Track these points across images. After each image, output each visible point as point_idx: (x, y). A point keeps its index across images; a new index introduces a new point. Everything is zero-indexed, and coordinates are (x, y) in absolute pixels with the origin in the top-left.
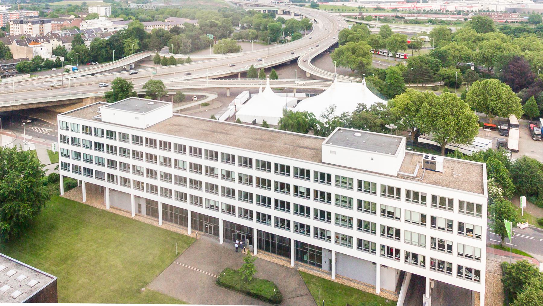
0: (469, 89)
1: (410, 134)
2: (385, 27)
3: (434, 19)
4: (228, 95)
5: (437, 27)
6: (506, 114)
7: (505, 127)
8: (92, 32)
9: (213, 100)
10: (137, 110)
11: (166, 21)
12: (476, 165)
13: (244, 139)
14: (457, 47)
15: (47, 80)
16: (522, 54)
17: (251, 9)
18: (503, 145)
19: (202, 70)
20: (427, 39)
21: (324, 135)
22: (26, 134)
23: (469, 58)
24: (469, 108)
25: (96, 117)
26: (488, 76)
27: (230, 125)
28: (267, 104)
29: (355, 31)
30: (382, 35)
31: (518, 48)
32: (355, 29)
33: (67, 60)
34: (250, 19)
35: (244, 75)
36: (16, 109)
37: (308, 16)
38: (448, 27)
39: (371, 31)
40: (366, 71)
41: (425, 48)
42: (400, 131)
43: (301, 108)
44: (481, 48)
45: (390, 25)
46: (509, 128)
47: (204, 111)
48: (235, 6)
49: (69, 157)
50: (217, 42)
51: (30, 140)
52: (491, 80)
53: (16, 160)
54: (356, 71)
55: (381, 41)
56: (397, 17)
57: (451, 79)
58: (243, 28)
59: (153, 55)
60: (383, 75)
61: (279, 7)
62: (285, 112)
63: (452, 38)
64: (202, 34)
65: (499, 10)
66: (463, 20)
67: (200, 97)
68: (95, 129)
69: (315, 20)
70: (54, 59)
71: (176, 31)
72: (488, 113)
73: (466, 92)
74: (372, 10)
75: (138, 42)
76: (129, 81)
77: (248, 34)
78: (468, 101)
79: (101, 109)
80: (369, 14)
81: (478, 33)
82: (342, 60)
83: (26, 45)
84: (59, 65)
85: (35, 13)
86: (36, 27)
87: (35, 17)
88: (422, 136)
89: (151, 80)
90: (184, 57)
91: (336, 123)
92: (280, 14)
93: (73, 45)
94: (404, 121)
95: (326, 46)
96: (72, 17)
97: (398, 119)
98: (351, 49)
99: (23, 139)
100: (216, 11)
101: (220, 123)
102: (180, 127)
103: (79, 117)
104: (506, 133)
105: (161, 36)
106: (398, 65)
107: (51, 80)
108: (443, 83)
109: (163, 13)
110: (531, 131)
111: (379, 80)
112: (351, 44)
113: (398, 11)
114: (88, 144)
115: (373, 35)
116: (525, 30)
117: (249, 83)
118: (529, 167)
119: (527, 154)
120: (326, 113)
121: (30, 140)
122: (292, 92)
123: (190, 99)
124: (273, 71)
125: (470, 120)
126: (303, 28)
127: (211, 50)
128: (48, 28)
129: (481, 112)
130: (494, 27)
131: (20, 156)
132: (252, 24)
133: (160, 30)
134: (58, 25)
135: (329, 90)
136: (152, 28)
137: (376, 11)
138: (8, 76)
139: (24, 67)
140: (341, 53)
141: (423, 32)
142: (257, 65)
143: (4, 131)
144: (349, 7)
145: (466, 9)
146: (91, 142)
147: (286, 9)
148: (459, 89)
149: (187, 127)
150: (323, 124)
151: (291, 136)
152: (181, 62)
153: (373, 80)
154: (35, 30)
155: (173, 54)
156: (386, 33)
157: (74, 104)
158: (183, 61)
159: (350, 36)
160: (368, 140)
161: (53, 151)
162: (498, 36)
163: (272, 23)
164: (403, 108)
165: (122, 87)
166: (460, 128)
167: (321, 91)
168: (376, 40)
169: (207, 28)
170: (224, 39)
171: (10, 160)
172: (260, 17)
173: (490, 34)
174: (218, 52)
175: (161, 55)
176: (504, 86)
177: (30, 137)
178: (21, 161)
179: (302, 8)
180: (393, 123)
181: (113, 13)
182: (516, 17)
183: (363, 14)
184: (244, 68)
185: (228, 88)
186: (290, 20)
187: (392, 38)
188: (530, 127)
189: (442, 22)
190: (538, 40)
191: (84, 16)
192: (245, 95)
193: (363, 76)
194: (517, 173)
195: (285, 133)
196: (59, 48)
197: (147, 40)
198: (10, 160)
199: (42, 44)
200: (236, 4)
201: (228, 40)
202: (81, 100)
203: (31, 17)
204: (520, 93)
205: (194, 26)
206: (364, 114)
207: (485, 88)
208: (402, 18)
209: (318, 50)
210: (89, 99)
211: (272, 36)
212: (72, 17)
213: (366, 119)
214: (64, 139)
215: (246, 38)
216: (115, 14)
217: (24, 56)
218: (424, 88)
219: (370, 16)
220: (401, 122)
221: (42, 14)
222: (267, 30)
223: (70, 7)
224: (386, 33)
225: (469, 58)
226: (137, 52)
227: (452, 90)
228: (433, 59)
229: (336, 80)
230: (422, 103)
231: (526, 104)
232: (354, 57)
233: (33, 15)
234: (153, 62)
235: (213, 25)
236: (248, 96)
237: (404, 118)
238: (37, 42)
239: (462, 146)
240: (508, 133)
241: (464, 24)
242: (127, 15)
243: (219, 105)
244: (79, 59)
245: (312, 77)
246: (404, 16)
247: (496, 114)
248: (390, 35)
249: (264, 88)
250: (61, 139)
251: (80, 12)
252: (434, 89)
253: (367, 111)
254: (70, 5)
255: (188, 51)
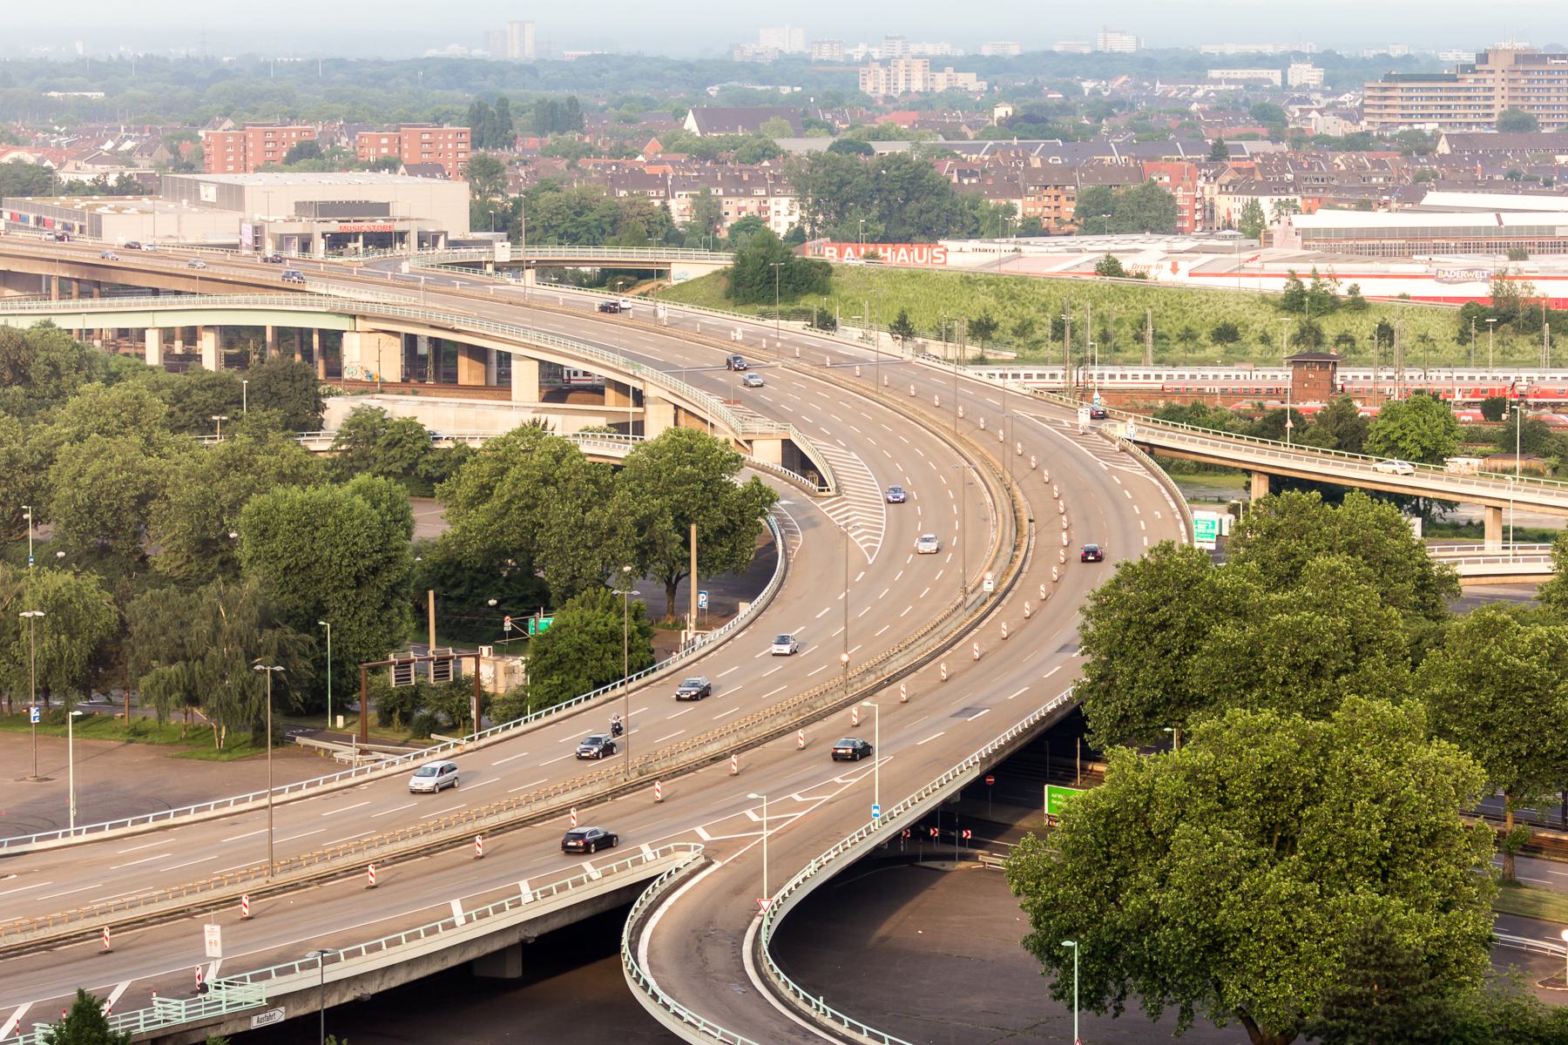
61: (363, 296)
69: (796, 459)
74: (1443, 329)
80: (1414, 378)
95: (941, 761)
98: (1242, 789)
112: (1245, 736)
137: (1489, 343)
144: (1178, 298)
151: (129, 251)
159: (1227, 632)
163: (296, 493)
168: (1513, 687)
172: (134, 416)
183: (1349, 376)
186: (503, 454)
209: (855, 810)
219: (1427, 402)
232: (1280, 881)
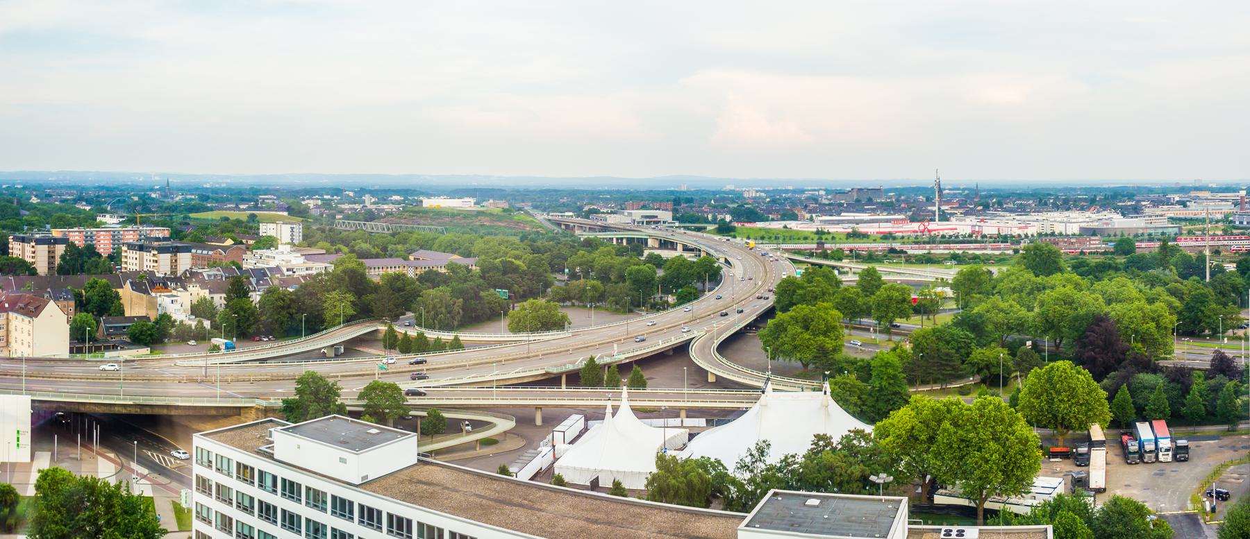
0: (1022, 385)
1: (920, 490)
2: (868, 270)
3: (960, 252)
4: (539, 422)
5: (965, 268)
6: (1084, 426)
7: (1083, 450)
8: (265, 275)
9: (505, 433)
10: (344, 443)
11: (411, 258)
12: (1036, 532)
13: (571, 521)
14: (1004, 305)
15: (179, 362)
16: (1107, 309)
17: (592, 235)
18: (1081, 483)
19: (478, 367)
20: (949, 292)
21: (746, 508)
22: (139, 463)
23: (1022, 325)
24: (1023, 422)
25: (263, 448)
26: (1054, 357)
27: (540, 488)
28: (618, 445)
29: (810, 282)
30: (864, 289)
31: (1101, 300)
32: (809, 276)
33: (215, 326)
34: (589, 257)
35: (574, 378)
36: (124, 411)
37: (712, 252)
38: (984, 269)
39: (841, 282)
40: (831, 364)
41: (944, 310)
42: (899, 485)
43: (700, 449)
44: (1042, 304)
45: (879, 267)
46: (1089, 450)
47: (488, 456)
48: (557, 229)
49: (210, 523)
50: (518, 306)
51: (144, 477)
52: (1060, 363)
53: (118, 510)
54: (811, 366)
55: (860, 301)
56: (892, 251)
57: (993, 370)
58: (573, 276)
59: (383, 328)
60: (865, 371)
61: (651, 232)
62: (661, 460)
63: (994, 288)
64: (487, 289)
65: (1069, 233)
66: (1011, 252)
67: (477, 425)
68: (261, 472)
69: (727, 261)
70: (193, 324)
71: (430, 278)
72: (1056, 428)
73: (1019, 391)
74: (843, 237)
75: (352, 299)
76: (331, 381)
77: (584, 290)
78: (1022, 409)
79: (274, 434)
81: (1037, 276)
82: (783, 344)
83: (146, 292)
84: (201, 336)
85: (161, 232)
86: (165, 258)
87: (165, 239)
88: (940, 491)
89: (376, 382)
90: (447, 336)
91: (772, 479)
92: (653, 248)
93: (228, 299)
94: (908, 464)
96: (229, 242)
97: (896, 461)
98: (800, 319)
99: (132, 471)
100: (516, 239)
101: (519, 484)
102: (431, 489)
103: (232, 444)
104: (1084, 461)
105: (399, 290)
106: (894, 349)
107: (186, 363)
108: (978, 378)
109: (404, 241)
110: (1124, 447)
111: (858, 383)
112: (802, 309)
113: (894, 238)
114: (247, 503)
115: (846, 290)
116: (1110, 267)
117: (586, 397)
118: (1122, 514)
119: (1119, 493)
120: (748, 460)
121: (144, 477)
122: (678, 416)
123: (455, 427)
124: (633, 372)
125: (1025, 445)
126: (700, 278)
127: (504, 323)
128: (185, 261)
129: (1045, 427)
130: (1062, 263)
131: (125, 502)
132: (592, 267)
133: (398, 277)
134: (203, 258)
135: (755, 408)
136: (381, 272)
137: (851, 240)
138: (115, 347)
139: (141, 333)
140: (780, 328)
141: (939, 278)
142: (601, 357)
143: (103, 450)
145: (1016, 232)
146: (252, 499)
147: (667, 235)
148: (1007, 388)
149: (447, 488)
150: (743, 485)
152: (439, 346)
153: (846, 384)
154: (161, 265)
155: (423, 330)
156: (870, 282)
157: (226, 416)
158: (444, 344)
159: (800, 292)
160: (833, 512)
161: (184, 505)
162: (1069, 281)
164: (904, 437)
165: (316, 393)
166: (1009, 464)
167: (738, 413)
168: (850, 300)
169: (498, 276)
170: (531, 300)
171: (109, 507)
172: (609, 253)
173: (1056, 278)
174: (517, 328)
175: (400, 330)
176: (1079, 373)
177: (145, 471)
178: (126, 512)
179: (700, 234)
180: (885, 471)
181: (305, 237)
182: (1095, 244)
183: (826, 246)
184: (573, 363)
185: (538, 407)
186: (673, 260)
187: (882, 293)
188: (1121, 442)
189: (975, 258)
190: (1129, 283)
191: (251, 242)
192: (574, 423)
193: (825, 376)
194: (1104, 530)
195: (660, 508)
196: (203, 302)
197: (370, 297)
198: (109, 507)
199: (174, 293)
200: (559, 225)
201: (541, 301)
202: (237, 411)
203: (158, 239)
204: (1105, 381)
205: (469, 271)
206: (827, 456)
207: (1050, 380)
208: (902, 252)
210: (253, 411)
211: (635, 293)
212: (229, 242)
213: (831, 468)
214: (204, 485)
215: (580, 299)
216: (308, 239)
217: (142, 313)
218: (945, 391)
220: (902, 466)
221: (176, 234)
222: (624, 281)
223: (225, 223)
224: (870, 282)
225: (1022, 325)
226: (350, 320)
227: (994, 390)
228: (957, 331)
229: (770, 386)
230: (940, 422)
231: (1115, 401)
233: (161, 236)
234: (381, 344)
235: (508, 269)
236: (581, 424)
237: (907, 458)
238: (166, 287)
239: (1013, 499)
240: (1088, 460)
241: (1013, 261)
242: (333, 243)
243: (517, 443)
244: (239, 326)
245: (721, 383)
246: (906, 248)
247: (1067, 428)
248: (878, 287)
249: (615, 410)
250: (198, 484)
251: (244, 233)
252: (963, 391)
253: (834, 450)
254: (227, 219)
255: (456, 323)
